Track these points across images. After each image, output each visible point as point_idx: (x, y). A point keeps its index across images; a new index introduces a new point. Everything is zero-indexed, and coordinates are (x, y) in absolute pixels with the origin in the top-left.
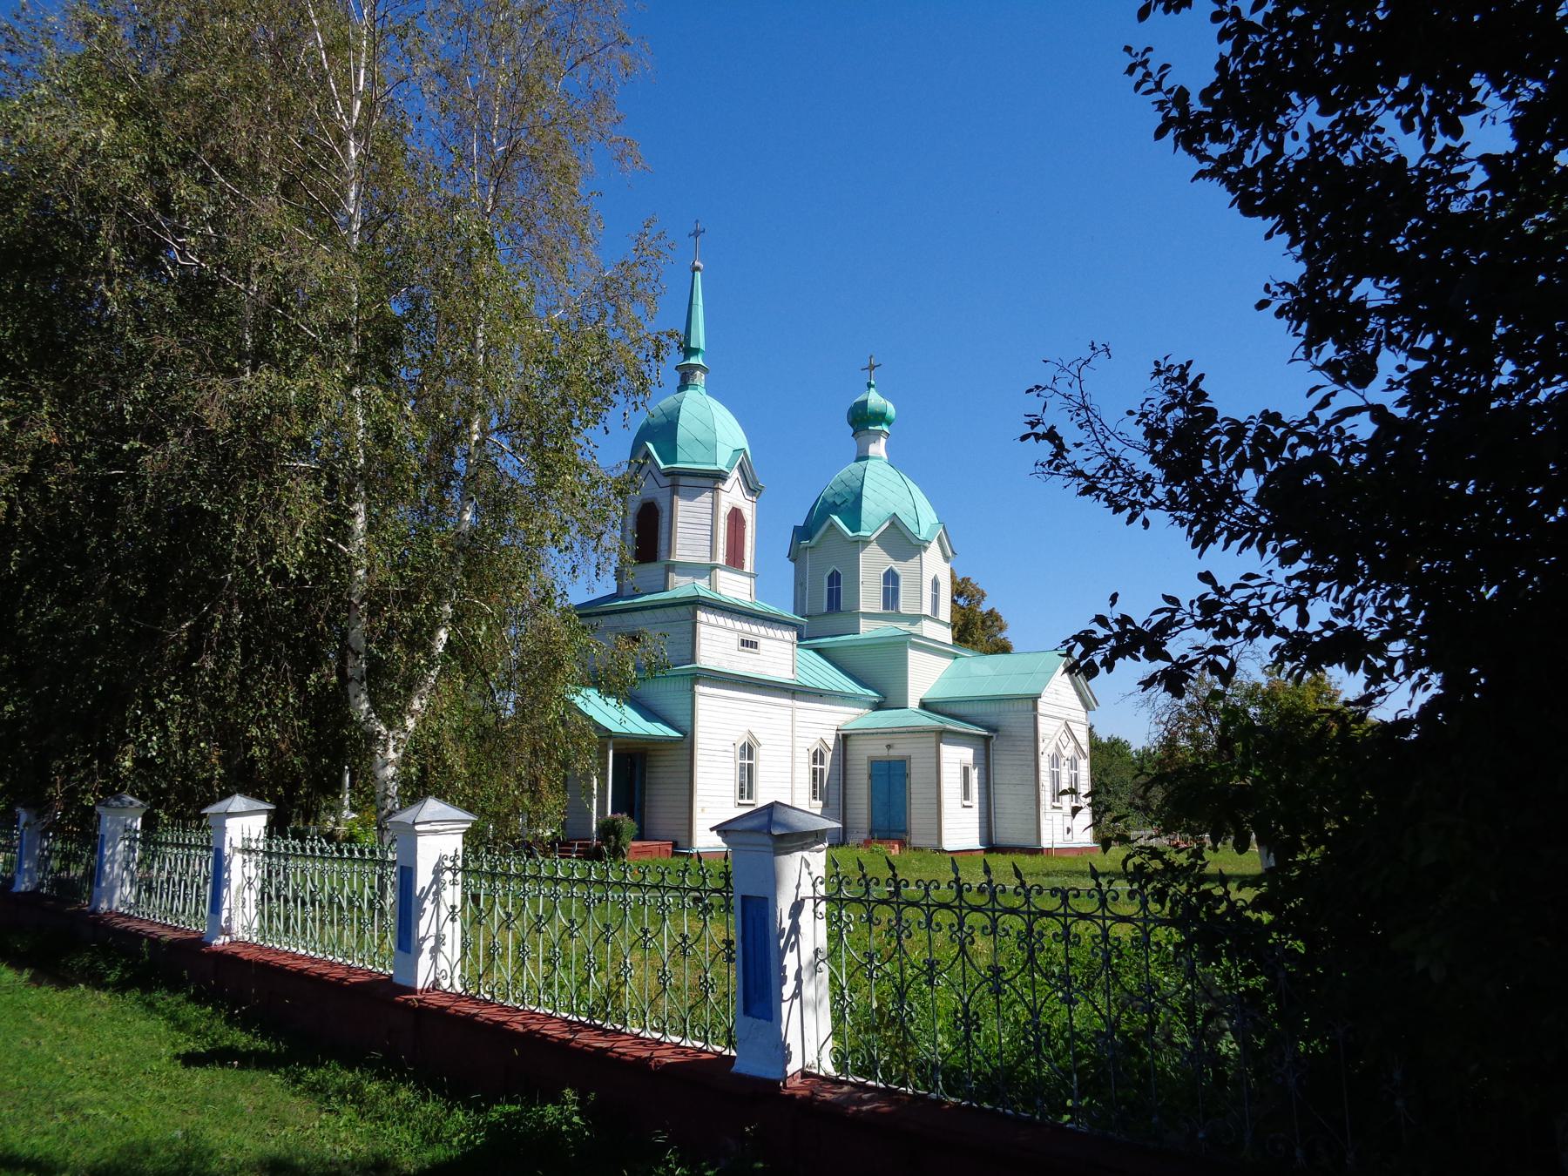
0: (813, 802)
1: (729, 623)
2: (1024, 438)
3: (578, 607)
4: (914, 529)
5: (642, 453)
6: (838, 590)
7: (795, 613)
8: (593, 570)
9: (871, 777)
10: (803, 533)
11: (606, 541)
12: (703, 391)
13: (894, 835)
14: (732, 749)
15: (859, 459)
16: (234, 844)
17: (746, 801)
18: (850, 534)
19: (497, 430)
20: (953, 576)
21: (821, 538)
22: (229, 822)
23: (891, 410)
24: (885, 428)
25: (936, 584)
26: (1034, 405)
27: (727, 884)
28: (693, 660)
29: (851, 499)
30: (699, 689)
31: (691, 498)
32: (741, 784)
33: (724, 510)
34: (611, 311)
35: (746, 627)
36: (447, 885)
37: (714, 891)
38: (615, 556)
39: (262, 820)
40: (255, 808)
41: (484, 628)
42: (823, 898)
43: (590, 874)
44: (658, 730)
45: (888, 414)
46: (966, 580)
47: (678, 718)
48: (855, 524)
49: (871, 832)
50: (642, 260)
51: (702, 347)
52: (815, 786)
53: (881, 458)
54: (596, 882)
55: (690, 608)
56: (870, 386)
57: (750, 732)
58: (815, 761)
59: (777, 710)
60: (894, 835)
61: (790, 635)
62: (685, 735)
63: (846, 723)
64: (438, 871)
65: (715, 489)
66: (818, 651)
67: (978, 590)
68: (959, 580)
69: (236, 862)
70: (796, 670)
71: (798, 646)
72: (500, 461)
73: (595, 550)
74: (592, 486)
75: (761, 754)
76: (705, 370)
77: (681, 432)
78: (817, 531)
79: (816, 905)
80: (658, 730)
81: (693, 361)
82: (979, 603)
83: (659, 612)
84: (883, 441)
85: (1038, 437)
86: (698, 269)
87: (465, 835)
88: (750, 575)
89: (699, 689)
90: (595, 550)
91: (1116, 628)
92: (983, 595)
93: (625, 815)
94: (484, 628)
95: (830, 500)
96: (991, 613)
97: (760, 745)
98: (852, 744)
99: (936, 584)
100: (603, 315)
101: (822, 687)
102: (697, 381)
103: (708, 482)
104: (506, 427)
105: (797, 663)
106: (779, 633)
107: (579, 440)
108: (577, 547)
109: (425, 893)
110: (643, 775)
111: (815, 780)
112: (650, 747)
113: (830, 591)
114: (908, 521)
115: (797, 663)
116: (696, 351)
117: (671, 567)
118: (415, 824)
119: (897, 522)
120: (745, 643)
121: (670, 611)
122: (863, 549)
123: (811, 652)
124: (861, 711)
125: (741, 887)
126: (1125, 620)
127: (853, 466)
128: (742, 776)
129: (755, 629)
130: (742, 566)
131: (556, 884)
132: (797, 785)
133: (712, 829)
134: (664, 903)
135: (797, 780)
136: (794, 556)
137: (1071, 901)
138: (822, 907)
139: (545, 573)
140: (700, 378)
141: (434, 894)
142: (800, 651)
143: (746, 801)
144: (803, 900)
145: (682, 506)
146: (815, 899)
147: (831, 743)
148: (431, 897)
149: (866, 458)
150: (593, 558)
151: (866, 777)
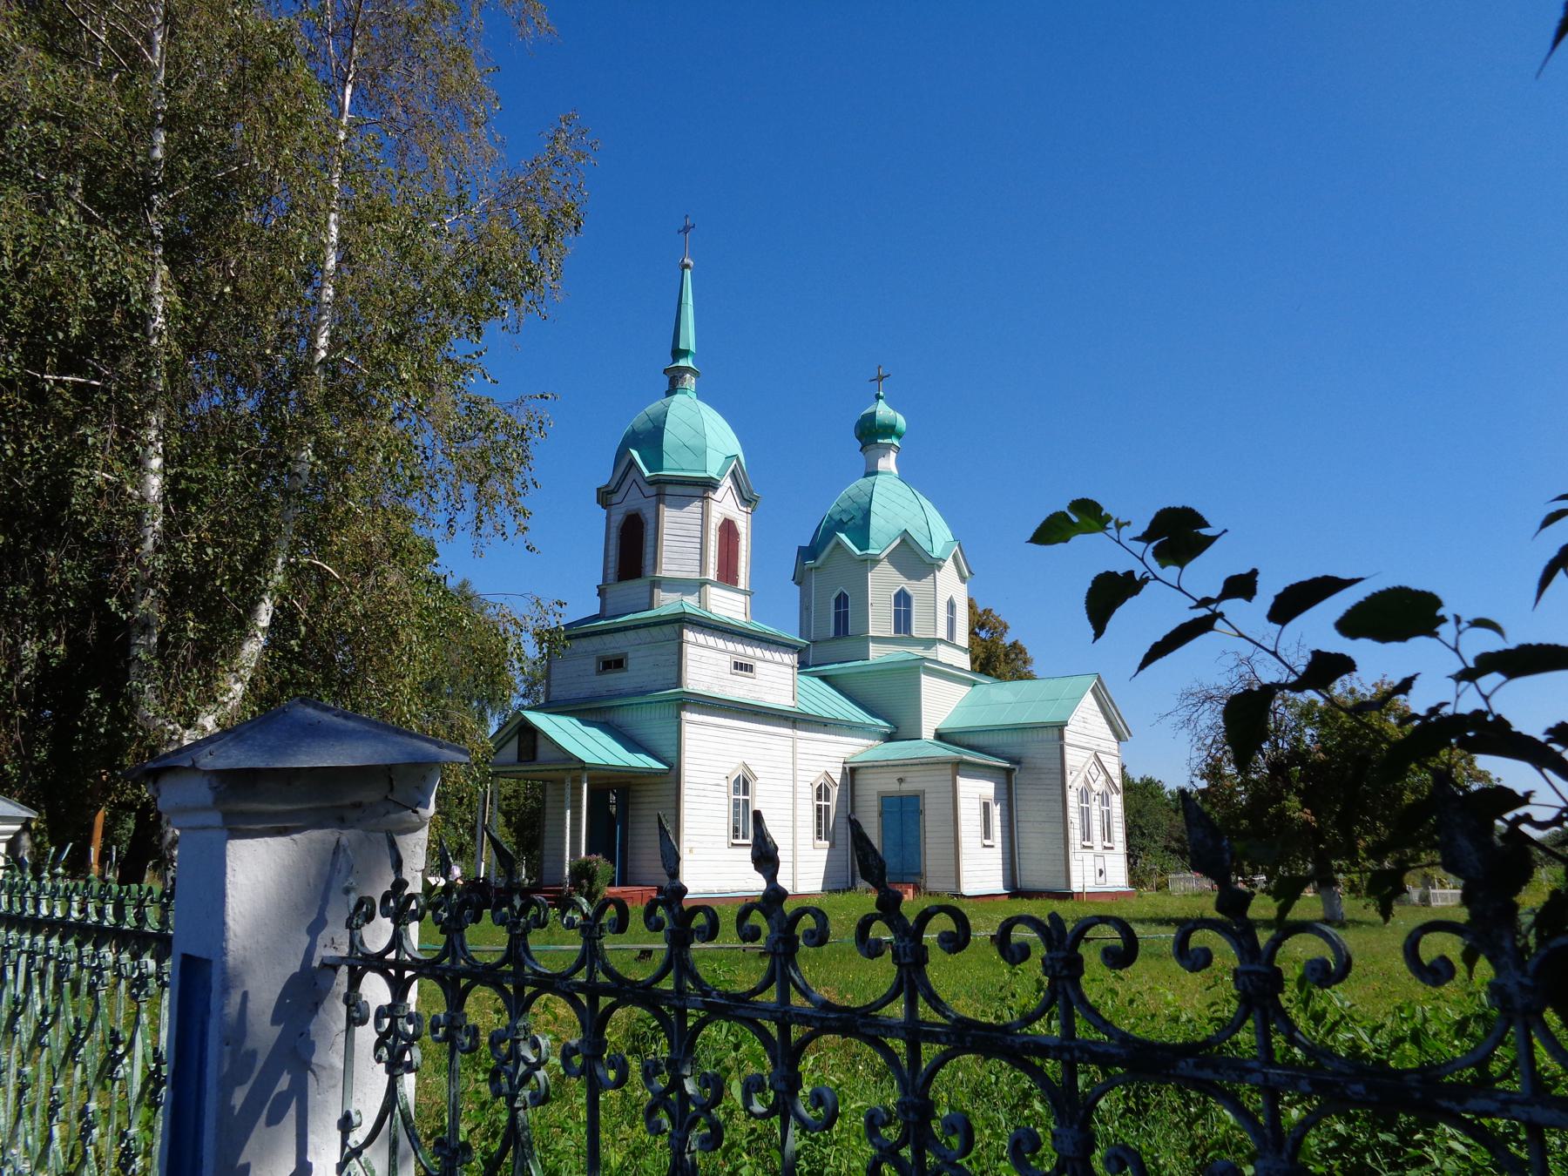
0: (818, 842)
1: (721, 643)
4: (926, 546)
6: (846, 613)
9: (881, 814)
10: (807, 553)
12: (694, 396)
14: (724, 783)
15: (867, 475)
18: (858, 552)
21: (829, 555)
23: (901, 422)
25: (951, 606)
28: (679, 683)
29: (859, 515)
30: (687, 716)
31: (681, 507)
33: (715, 521)
35: (740, 648)
46: (988, 612)
48: (863, 542)
51: (692, 348)
52: (819, 825)
53: (891, 473)
55: (676, 626)
56: (878, 397)
59: (776, 740)
61: (790, 659)
62: (671, 766)
63: (854, 755)
65: (704, 499)
67: (1000, 623)
68: (980, 610)
70: (798, 697)
77: (667, 437)
78: (824, 548)
81: (682, 363)
82: (1002, 635)
83: (643, 632)
84: (893, 455)
86: (687, 266)
88: (744, 592)
89: (687, 716)
92: (1006, 627)
95: (837, 517)
96: (1014, 645)
97: (756, 778)
98: (859, 777)
99: (951, 606)
101: (826, 715)
102: (686, 385)
103: (698, 491)
106: (777, 656)
111: (819, 818)
112: (633, 781)
113: (837, 615)
116: (686, 353)
117: (657, 583)
119: (909, 540)
120: (739, 666)
121: (655, 631)
122: (872, 568)
124: (871, 742)
127: (861, 481)
129: (749, 650)
130: (735, 582)
132: (799, 824)
136: (800, 578)
140: (690, 382)
142: (803, 678)
143: (740, 841)
145: (669, 515)
147: (837, 777)
149: (876, 473)
151: (876, 814)
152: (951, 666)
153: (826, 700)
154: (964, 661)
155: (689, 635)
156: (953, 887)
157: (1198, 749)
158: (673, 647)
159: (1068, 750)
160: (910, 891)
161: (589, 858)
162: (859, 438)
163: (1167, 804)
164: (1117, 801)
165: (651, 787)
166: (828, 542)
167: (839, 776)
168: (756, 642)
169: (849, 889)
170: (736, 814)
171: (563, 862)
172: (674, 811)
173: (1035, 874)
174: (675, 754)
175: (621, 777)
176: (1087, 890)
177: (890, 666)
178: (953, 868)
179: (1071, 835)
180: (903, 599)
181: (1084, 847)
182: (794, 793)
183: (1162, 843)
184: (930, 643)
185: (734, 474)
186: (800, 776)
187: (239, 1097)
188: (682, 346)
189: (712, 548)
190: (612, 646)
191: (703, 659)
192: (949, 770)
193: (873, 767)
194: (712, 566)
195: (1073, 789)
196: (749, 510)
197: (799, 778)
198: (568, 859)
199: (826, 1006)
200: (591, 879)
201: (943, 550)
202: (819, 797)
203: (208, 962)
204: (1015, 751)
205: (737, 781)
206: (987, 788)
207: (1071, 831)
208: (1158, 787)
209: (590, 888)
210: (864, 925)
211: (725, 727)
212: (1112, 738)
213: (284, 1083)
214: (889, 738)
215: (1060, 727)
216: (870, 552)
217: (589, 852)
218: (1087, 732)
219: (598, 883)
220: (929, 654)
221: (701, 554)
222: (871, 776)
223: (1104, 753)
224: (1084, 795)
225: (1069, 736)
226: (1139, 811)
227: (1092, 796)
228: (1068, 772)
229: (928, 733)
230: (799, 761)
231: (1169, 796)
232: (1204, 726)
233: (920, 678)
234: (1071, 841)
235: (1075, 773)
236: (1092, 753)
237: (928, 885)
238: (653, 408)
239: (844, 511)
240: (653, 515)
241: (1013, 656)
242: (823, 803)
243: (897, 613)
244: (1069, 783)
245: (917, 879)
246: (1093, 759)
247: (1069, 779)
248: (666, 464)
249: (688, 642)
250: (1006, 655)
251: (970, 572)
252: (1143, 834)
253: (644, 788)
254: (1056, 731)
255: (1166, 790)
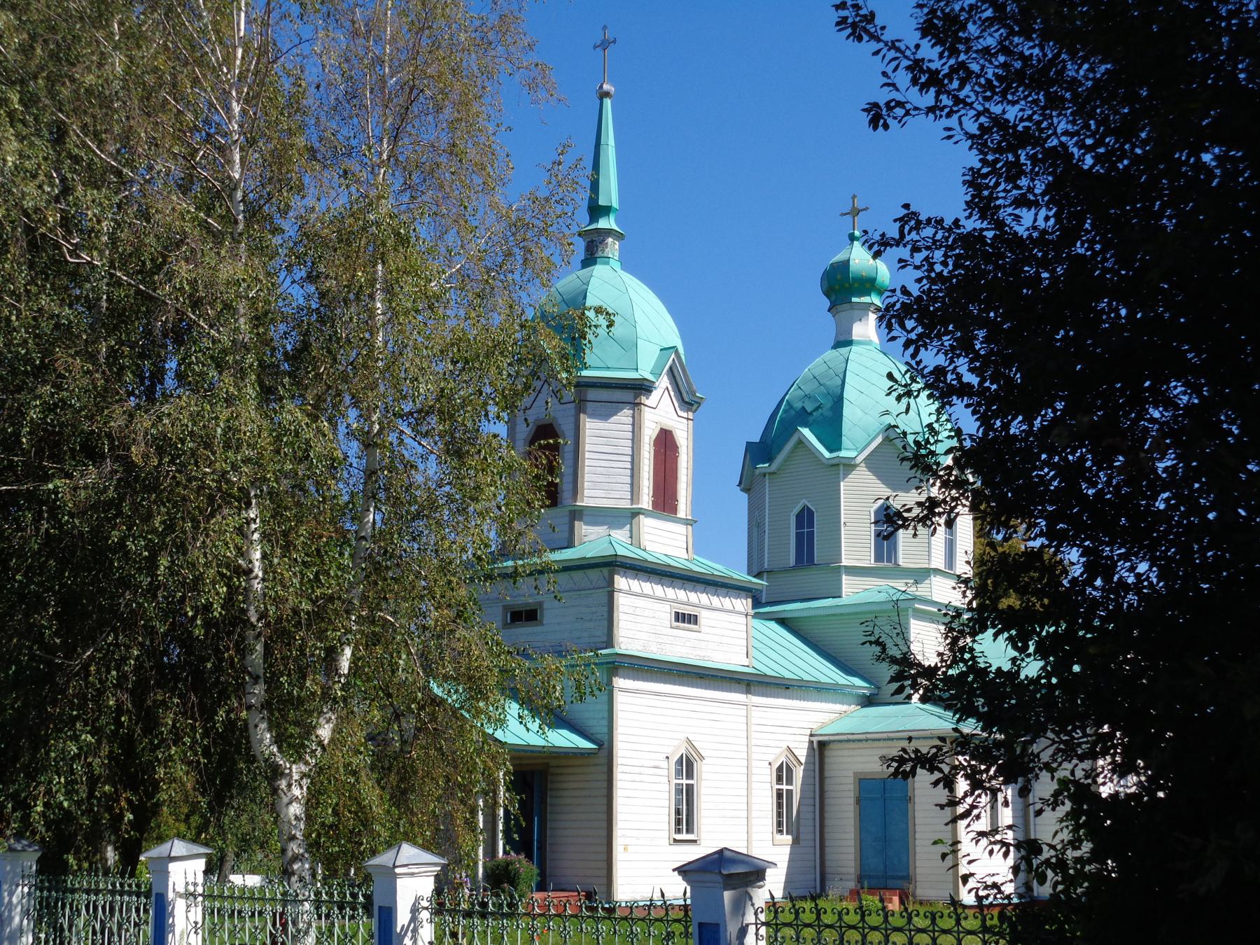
0: (778, 837)
1: (658, 590)
2: (863, 644)
6: (811, 534)
7: (749, 574)
9: (859, 801)
10: (760, 452)
12: (617, 266)
13: (890, 883)
14: (664, 764)
16: (178, 889)
17: (684, 836)
18: (827, 454)
21: (786, 460)
22: (173, 867)
26: (863, 628)
27: (686, 915)
28: (609, 643)
29: (828, 404)
30: (619, 682)
31: (605, 416)
32: (678, 812)
33: (649, 433)
35: (682, 594)
36: (425, 923)
37: (675, 921)
39: (200, 864)
40: (195, 852)
41: (404, 656)
42: (763, 924)
43: (565, 910)
44: (563, 739)
45: (879, 279)
47: (591, 723)
48: (834, 442)
49: (860, 879)
51: (615, 204)
52: (779, 815)
53: (869, 343)
54: (572, 916)
55: (605, 571)
56: (852, 238)
57: (688, 740)
58: (779, 780)
59: (726, 709)
60: (890, 883)
61: (743, 604)
62: (600, 744)
63: (823, 725)
64: (415, 910)
65: (636, 405)
66: (783, 622)
69: (180, 906)
70: (753, 652)
71: (756, 616)
75: (704, 771)
76: (619, 236)
78: (780, 449)
79: (757, 930)
80: (563, 739)
81: (603, 224)
85: (871, 643)
86: (607, 94)
87: (437, 877)
88: (686, 522)
89: (619, 682)
91: (913, 756)
93: (522, 857)
94: (404, 656)
95: (798, 405)
97: (702, 758)
98: (833, 756)
101: (788, 675)
103: (627, 395)
105: (753, 642)
106: (727, 602)
109: (405, 930)
110: (543, 801)
111: (779, 805)
112: (553, 762)
113: (799, 537)
115: (753, 632)
116: (606, 211)
117: (577, 514)
118: (395, 867)
120: (681, 618)
121: (578, 575)
122: (846, 476)
123: (773, 625)
124: (845, 708)
125: (696, 917)
126: (917, 751)
127: (831, 354)
128: (678, 802)
129: (693, 597)
130: (674, 510)
131: (534, 919)
132: (754, 814)
133: (674, 870)
134: (632, 932)
135: (754, 807)
136: (748, 483)
137: (938, 920)
138: (763, 931)
140: (612, 247)
141: (412, 931)
142: (757, 623)
143: (684, 836)
144: (747, 925)
145: (592, 428)
146: (756, 924)
147: (802, 754)
148: (409, 934)
149: (849, 343)
151: (852, 801)
153: (786, 654)
155: (621, 582)
158: (602, 595)
166: (787, 440)
167: (805, 752)
168: (702, 586)
172: (604, 801)
174: (605, 730)
175: (535, 758)
185: (672, 372)
188: (602, 202)
189: (646, 462)
190: (524, 594)
191: (638, 611)
193: (848, 741)
196: (691, 415)
197: (754, 756)
216: (843, 454)
221: (632, 476)
222: (846, 753)
230: (754, 735)
239: (807, 396)
240: (572, 426)
242: (785, 787)
245: (905, 885)
248: (589, 358)
249: (620, 591)
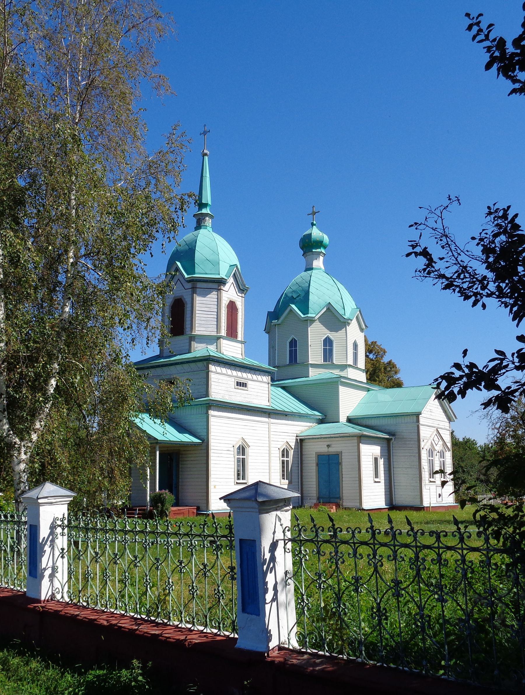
0: (283, 481)
1: (229, 372)
3: (136, 364)
4: (341, 312)
5: (174, 268)
7: (269, 365)
8: (145, 341)
9: (318, 465)
10: (273, 315)
11: (152, 322)
12: (211, 230)
14: (232, 449)
18: (302, 316)
19: (84, 255)
20: (366, 341)
21: (286, 317)
23: (326, 239)
24: (323, 250)
25: (355, 346)
28: (207, 395)
29: (303, 294)
30: (211, 412)
31: (204, 295)
33: (225, 303)
34: (153, 182)
35: (239, 374)
38: (158, 332)
48: (305, 309)
50: (172, 150)
51: (210, 202)
52: (283, 471)
53: (320, 269)
55: (205, 363)
56: (313, 224)
62: (203, 441)
63: (302, 432)
65: (219, 290)
67: (381, 349)
68: (369, 343)
70: (271, 400)
72: (86, 274)
73: (146, 328)
74: (143, 289)
76: (211, 217)
78: (282, 314)
81: (204, 211)
82: (382, 357)
83: (186, 366)
84: (321, 258)
86: (206, 154)
88: (241, 342)
89: (211, 412)
90: (146, 328)
92: (385, 352)
95: (290, 295)
96: (390, 363)
97: (249, 446)
99: (355, 346)
100: (148, 184)
101: (286, 410)
102: (207, 223)
103: (215, 286)
104: (90, 254)
106: (259, 378)
107: (135, 261)
108: (134, 326)
111: (283, 467)
112: (182, 449)
113: (291, 351)
114: (338, 307)
116: (205, 205)
117: (193, 338)
119: (331, 308)
120: (239, 384)
121: (193, 365)
124: (311, 424)
127: (304, 274)
129: (245, 375)
130: (236, 337)
132: (272, 471)
136: (268, 330)
139: (116, 343)
140: (208, 222)
142: (273, 388)
145: (199, 300)
147: (293, 445)
149: (311, 269)
150: (145, 333)
151: (315, 465)
152: (355, 381)
154: (362, 377)
155: (212, 368)
156: (358, 505)
157: (493, 429)
159: (421, 428)
160: (334, 507)
161: (161, 492)
162: (302, 249)
163: (478, 454)
164: (448, 456)
165: (191, 452)
167: (294, 444)
168: (248, 370)
169: (301, 507)
170: (238, 466)
171: (147, 494)
173: (401, 499)
174: (205, 434)
176: (432, 505)
177: (321, 381)
178: (358, 494)
179: (423, 476)
180: (328, 343)
181: (430, 482)
182: (269, 454)
183: (475, 476)
184: (344, 367)
185: (234, 275)
186: (273, 444)
187: (265, 567)
188: (204, 201)
191: (220, 381)
192: (355, 440)
193: (313, 438)
194: (223, 328)
195: (425, 450)
196: (243, 295)
197: (272, 446)
198: (148, 492)
199: (402, 544)
200: (163, 504)
201: (351, 314)
202: (283, 456)
203: (254, 541)
204: (392, 429)
205: (239, 448)
206: (376, 450)
207: (423, 473)
208: (474, 443)
209: (162, 508)
210: (311, 528)
211: (232, 418)
212: (446, 420)
213: (271, 565)
214: (321, 421)
215: (417, 415)
217: (160, 489)
218: (432, 417)
219: (167, 505)
220: (343, 374)
221: (217, 321)
222: (311, 444)
223: (442, 429)
224: (431, 453)
225: (422, 420)
226: (461, 458)
227: (435, 453)
228: (422, 440)
229: (343, 419)
230: (272, 436)
231: (479, 449)
232: (495, 417)
233: (338, 388)
234: (423, 479)
235: (425, 441)
236: (435, 429)
237: (344, 504)
238: (189, 237)
241: (389, 369)
242: (285, 459)
243: (325, 350)
244: (422, 446)
246: (435, 433)
247: (422, 444)
248: (197, 270)
249: (212, 372)
250: (385, 369)
251: (366, 326)
252: (464, 471)
253: (189, 452)
254: (415, 418)
255: (478, 445)
